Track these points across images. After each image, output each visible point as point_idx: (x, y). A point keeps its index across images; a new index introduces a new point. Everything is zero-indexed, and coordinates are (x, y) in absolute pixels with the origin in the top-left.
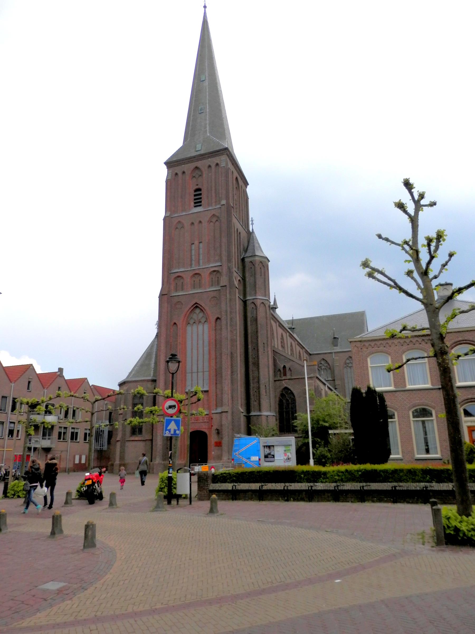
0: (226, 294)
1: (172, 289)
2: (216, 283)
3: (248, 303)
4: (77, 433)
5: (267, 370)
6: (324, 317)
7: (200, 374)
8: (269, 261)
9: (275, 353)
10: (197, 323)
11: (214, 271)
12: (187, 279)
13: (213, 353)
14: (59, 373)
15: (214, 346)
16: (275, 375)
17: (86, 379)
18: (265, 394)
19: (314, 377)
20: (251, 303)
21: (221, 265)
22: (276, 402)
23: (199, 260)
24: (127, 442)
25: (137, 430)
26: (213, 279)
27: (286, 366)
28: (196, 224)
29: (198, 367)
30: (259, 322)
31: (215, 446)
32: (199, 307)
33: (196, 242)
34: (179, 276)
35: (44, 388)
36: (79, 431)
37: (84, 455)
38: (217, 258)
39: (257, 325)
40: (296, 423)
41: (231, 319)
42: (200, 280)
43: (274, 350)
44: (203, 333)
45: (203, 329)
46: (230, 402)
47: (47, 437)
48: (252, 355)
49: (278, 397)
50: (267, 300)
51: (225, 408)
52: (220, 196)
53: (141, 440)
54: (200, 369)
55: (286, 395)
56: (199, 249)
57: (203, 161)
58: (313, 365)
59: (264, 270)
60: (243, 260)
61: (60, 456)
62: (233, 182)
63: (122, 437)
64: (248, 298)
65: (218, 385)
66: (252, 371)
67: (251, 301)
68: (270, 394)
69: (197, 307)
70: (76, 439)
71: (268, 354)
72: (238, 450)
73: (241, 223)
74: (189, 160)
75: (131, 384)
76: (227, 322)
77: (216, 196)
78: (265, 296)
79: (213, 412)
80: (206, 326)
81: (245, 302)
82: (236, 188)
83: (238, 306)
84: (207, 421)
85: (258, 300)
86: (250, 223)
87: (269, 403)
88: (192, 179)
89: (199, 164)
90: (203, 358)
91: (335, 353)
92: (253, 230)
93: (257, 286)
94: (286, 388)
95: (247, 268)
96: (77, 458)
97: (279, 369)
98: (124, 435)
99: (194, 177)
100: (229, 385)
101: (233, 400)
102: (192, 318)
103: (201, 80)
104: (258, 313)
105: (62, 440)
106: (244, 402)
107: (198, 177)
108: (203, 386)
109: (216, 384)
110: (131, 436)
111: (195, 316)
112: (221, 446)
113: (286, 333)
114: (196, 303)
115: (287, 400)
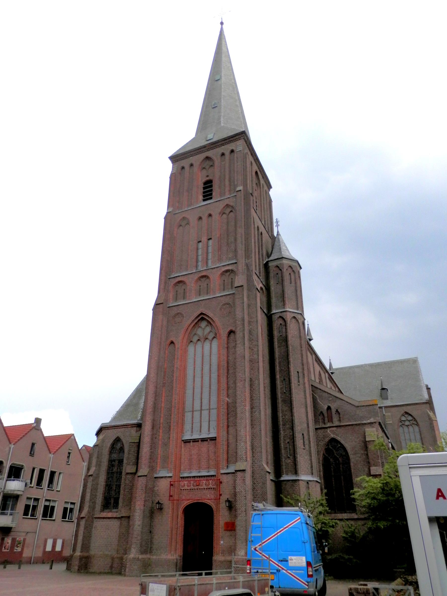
0: (243, 297)
1: (171, 297)
2: (230, 286)
3: (275, 317)
4: (53, 507)
5: (303, 410)
6: (366, 365)
7: (205, 413)
8: (301, 268)
9: (314, 389)
10: (202, 340)
11: (227, 271)
12: (191, 282)
13: (224, 380)
14: (35, 425)
15: (225, 371)
16: (316, 421)
17: (73, 435)
18: (303, 447)
19: (375, 422)
20: (278, 318)
21: (236, 263)
22: (319, 463)
23: (207, 259)
24: (95, 520)
25: (112, 501)
26: (225, 282)
27: (332, 407)
28: (205, 218)
29: (201, 403)
30: (290, 343)
31: (225, 530)
32: (205, 319)
33: (204, 239)
34: (180, 282)
35: (10, 443)
36: (56, 505)
37: (61, 538)
38: (231, 255)
39: (287, 347)
40: (358, 494)
41: (250, 332)
42: (207, 284)
43: (313, 384)
44: (211, 354)
45: (211, 348)
46: (249, 454)
47: (9, 511)
48: (281, 388)
49: (322, 453)
50: (301, 314)
51: (240, 466)
52: (236, 183)
53: (266, 528)
54: (205, 406)
55: (334, 451)
56: (208, 247)
57: (214, 150)
58: (373, 405)
59: (295, 276)
60: (266, 266)
61: (24, 540)
62: (252, 186)
63: (89, 512)
64: (274, 311)
65: (230, 428)
66: (283, 411)
67: (278, 315)
68: (310, 447)
69: (203, 319)
70: (51, 516)
71: (305, 387)
72: (260, 539)
73: (263, 223)
74: (198, 151)
75: (109, 431)
76: (244, 334)
77: (230, 185)
78: (298, 309)
79: (222, 471)
80: (215, 343)
81: (269, 317)
82: (257, 184)
83: (261, 319)
84: (212, 487)
85: (288, 313)
86: (275, 224)
87: (309, 462)
88: (201, 171)
89: (209, 154)
90: (210, 388)
91: (386, 407)
92: (278, 232)
93: (286, 295)
94: (333, 440)
95: (272, 275)
96: (50, 543)
97: (322, 412)
98: (92, 508)
99: (204, 168)
100: (248, 427)
101: (253, 452)
102: (195, 334)
103: (216, 80)
104: (289, 331)
105: (29, 517)
106: (270, 457)
107: (209, 168)
108: (209, 431)
109: (228, 427)
110: (102, 511)
111: (199, 332)
112: (235, 530)
113: (325, 373)
114: (202, 314)
115: (336, 459)
